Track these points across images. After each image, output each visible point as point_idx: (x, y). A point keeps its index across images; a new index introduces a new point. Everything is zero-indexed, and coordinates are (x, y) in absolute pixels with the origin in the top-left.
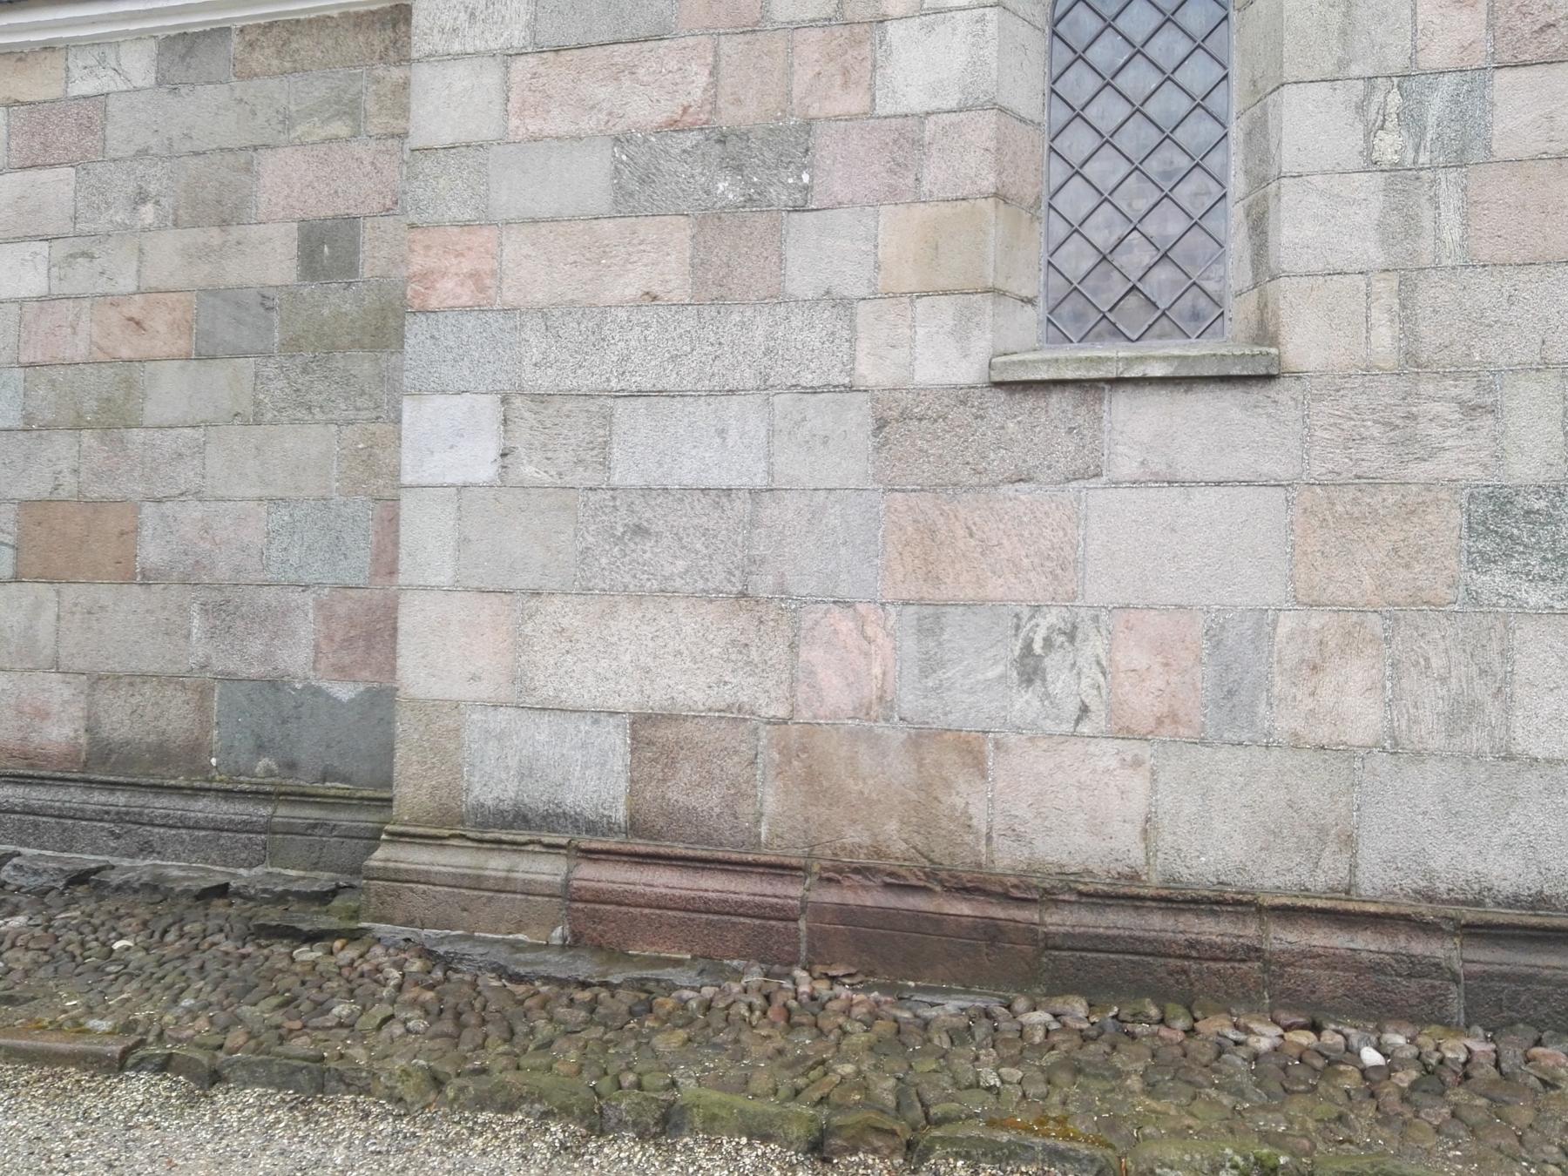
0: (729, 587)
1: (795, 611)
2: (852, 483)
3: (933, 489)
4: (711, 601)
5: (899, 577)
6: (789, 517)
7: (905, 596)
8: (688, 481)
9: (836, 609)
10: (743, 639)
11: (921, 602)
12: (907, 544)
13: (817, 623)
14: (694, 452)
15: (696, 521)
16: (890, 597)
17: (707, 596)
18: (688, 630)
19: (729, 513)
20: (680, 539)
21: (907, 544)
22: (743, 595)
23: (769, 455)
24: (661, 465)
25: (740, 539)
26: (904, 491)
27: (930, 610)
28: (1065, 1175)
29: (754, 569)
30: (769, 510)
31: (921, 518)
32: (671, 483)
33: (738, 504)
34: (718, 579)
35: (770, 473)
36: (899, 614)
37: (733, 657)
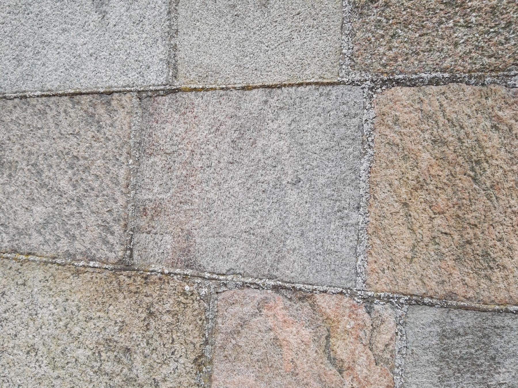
0: (104, 252)
1: (206, 298)
2: (312, 73)
3: (477, 78)
4: (77, 273)
5: (403, 249)
6: (201, 136)
7: (414, 287)
8: (53, 84)
9: (279, 302)
10: (122, 340)
11: (447, 302)
12: (420, 186)
13: (244, 323)
14: (62, 39)
15: (61, 144)
16: (382, 285)
17: (72, 264)
18: (44, 314)
19: (108, 131)
20: (40, 173)
21: (420, 186)
22: (125, 266)
23: (173, 33)
24: (20, 63)
25: (122, 173)
26: (412, 83)
27: (469, 319)
28: (293, 387)
29: (143, 222)
30: (171, 125)
31: (449, 134)
32: (30, 87)
33: (121, 114)
34: (88, 238)
35: (172, 63)
36: (401, 323)
37: (108, 367)
